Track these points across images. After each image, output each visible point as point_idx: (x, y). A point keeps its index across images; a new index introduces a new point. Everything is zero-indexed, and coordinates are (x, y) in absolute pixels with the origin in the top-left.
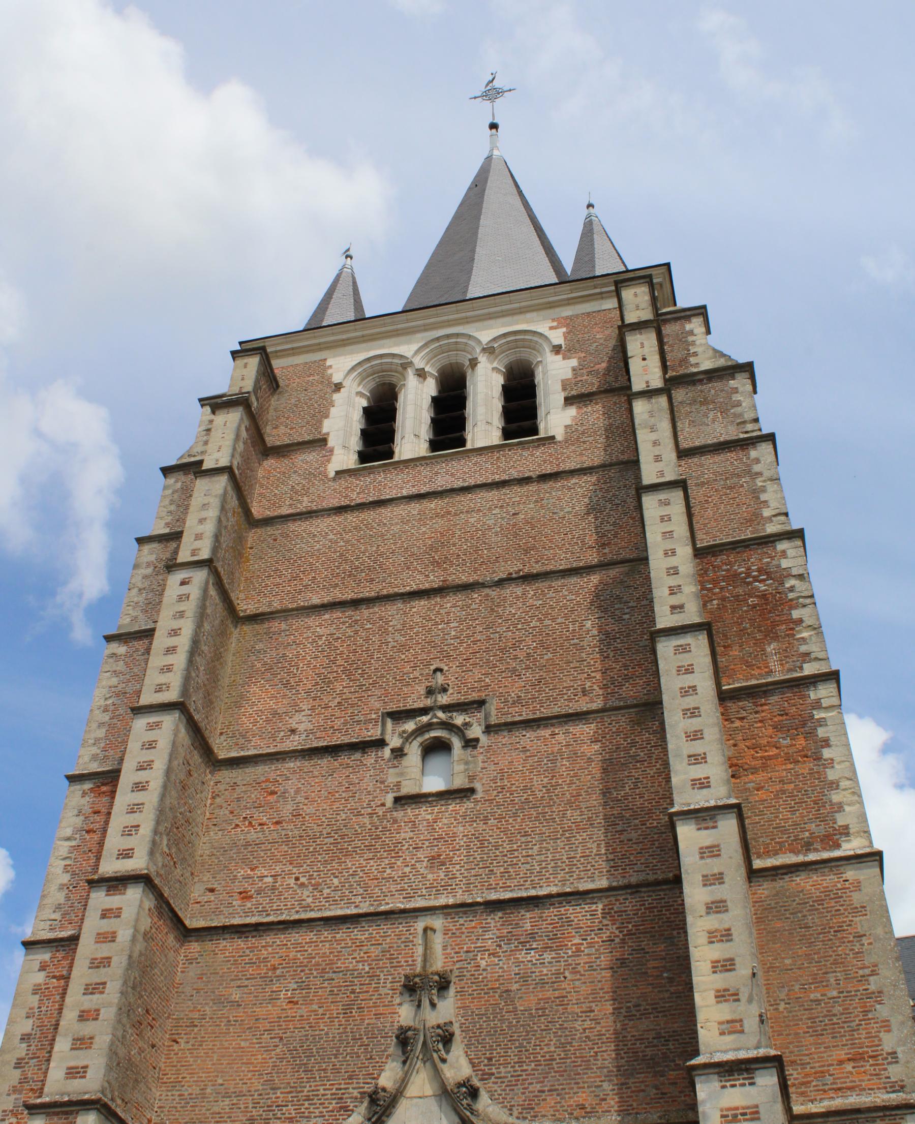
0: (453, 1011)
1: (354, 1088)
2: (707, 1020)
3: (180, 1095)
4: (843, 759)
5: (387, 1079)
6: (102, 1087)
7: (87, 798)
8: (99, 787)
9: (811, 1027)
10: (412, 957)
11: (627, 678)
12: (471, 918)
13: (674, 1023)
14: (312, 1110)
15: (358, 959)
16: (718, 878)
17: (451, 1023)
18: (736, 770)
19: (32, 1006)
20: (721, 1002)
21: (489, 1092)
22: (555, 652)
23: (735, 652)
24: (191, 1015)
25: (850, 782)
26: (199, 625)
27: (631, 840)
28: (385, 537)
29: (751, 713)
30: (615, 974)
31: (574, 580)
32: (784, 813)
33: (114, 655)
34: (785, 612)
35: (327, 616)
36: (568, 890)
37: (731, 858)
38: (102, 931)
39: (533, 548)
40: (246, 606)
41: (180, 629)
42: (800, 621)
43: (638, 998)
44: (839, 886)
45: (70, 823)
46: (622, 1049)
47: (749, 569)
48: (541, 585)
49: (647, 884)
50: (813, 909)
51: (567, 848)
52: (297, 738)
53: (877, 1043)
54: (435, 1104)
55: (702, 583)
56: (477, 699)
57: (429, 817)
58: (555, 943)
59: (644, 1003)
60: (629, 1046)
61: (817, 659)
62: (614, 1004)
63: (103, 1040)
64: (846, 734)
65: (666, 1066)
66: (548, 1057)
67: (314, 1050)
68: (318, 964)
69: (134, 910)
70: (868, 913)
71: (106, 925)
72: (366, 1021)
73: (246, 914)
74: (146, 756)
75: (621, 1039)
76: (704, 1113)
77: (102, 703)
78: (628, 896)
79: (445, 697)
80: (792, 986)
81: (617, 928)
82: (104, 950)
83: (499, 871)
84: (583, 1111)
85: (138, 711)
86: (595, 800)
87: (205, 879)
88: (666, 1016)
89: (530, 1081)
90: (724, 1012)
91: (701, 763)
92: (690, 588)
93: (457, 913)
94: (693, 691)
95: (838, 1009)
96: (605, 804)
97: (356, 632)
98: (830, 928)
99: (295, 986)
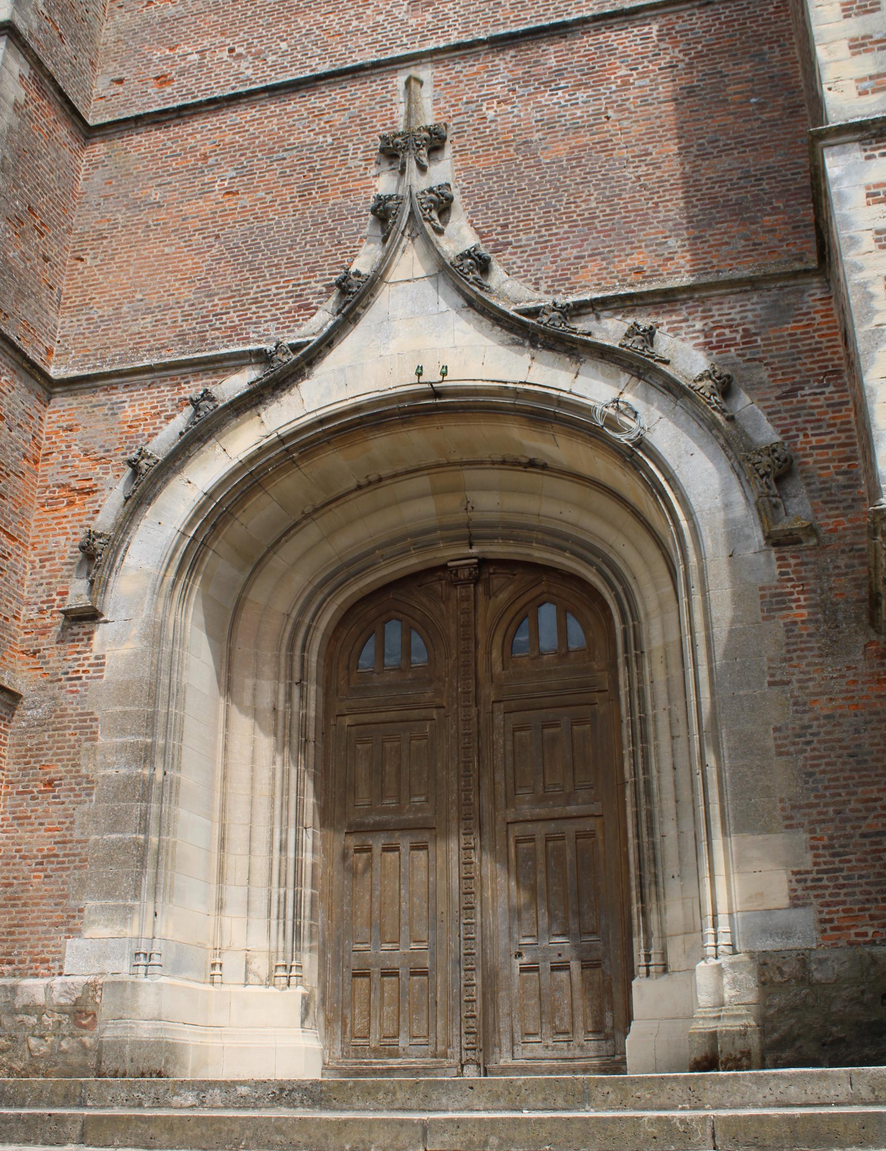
0: (450, 175)
1: (316, 282)
2: (838, 79)
3: (87, 320)
10: (391, 118)
12: (471, 63)
13: (768, 158)
14: (261, 314)
15: (317, 130)
17: (448, 185)
20: (859, 53)
21: (504, 265)
24: (98, 227)
30: (681, 107)
43: (714, 132)
46: (694, 196)
54: (430, 286)
59: (724, 137)
60: (704, 191)
62: (680, 143)
65: (759, 211)
66: (587, 215)
67: (262, 244)
68: (263, 144)
72: (331, 202)
75: (691, 183)
76: (840, 194)
78: (696, 11)
81: (680, 51)
87: (110, 70)
88: (756, 150)
89: (562, 246)
93: (452, 59)
99: (234, 174)
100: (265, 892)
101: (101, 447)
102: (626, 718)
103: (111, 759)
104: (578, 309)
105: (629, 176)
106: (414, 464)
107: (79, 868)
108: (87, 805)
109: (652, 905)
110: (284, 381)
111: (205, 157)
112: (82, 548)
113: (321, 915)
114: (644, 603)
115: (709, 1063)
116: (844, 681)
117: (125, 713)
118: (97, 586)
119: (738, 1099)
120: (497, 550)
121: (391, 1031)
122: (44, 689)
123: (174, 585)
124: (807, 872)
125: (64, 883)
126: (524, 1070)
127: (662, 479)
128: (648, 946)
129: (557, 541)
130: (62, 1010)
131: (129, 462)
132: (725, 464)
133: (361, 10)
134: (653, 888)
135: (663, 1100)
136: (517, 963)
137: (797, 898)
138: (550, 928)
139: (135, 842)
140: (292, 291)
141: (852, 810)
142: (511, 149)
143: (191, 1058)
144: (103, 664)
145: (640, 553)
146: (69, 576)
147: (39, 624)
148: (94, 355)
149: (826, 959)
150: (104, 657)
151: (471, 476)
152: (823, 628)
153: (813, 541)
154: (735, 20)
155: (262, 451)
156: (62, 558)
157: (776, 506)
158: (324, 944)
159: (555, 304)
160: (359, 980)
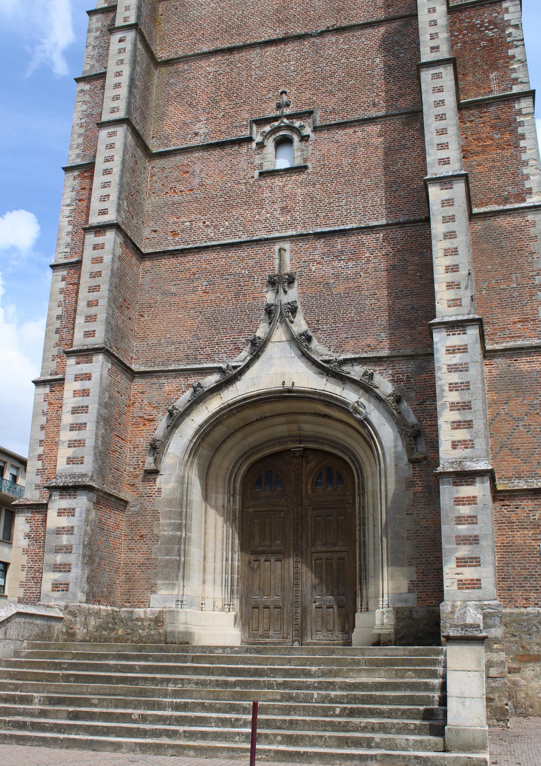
2: (441, 299)
3: (147, 344)
4: (532, 147)
5: (261, 332)
6: (104, 341)
7: (77, 181)
8: (83, 173)
9: (500, 304)
11: (401, 96)
16: (452, 218)
17: (296, 301)
18: (466, 153)
19: (60, 300)
20: (450, 289)
22: (356, 79)
23: (470, 78)
24: (149, 302)
25: (536, 161)
26: (133, 69)
27: (400, 196)
28: (247, 4)
29: (477, 118)
31: (369, 31)
32: (493, 180)
33: (82, 91)
34: (504, 51)
35: (213, 60)
36: (363, 226)
37: (460, 206)
38: (95, 257)
39: (343, 9)
40: (162, 55)
41: (122, 71)
42: (513, 57)
44: (523, 224)
45: (68, 196)
47: (483, 21)
48: (348, 35)
49: (410, 222)
50: (506, 237)
51: (362, 202)
52: (199, 138)
53: (536, 313)
55: (451, 32)
56: (308, 110)
57: (280, 184)
58: (355, 256)
60: (396, 313)
61: (522, 83)
63: (102, 316)
64: (535, 131)
68: (219, 271)
69: (112, 244)
70: (538, 240)
71: (97, 253)
72: (248, 302)
73: (176, 244)
74: (109, 153)
76: (437, 349)
77: (79, 121)
78: (398, 229)
79: (288, 110)
80: (491, 281)
81: (391, 248)
82: (97, 268)
83: (322, 215)
84: (370, 348)
85: (102, 125)
86: (380, 172)
88: (417, 297)
90: (452, 294)
91: (445, 149)
92: (444, 35)
93: (298, 240)
94: (442, 103)
95: (516, 294)
96: (386, 174)
97: (232, 69)
98: (515, 248)
99: (207, 283)
100: (220, 576)
101: (156, 402)
102: (358, 516)
103: (165, 528)
104: (345, 361)
105: (368, 304)
106: (279, 412)
107: (155, 569)
108: (157, 546)
109: (364, 587)
110: (230, 381)
111: (194, 274)
112: (151, 445)
113: (240, 585)
114: (366, 472)
115: (377, 643)
116: (432, 515)
117: (170, 511)
118: (157, 461)
119: (374, 654)
120: (311, 446)
121: (267, 628)
122: (137, 500)
123: (188, 460)
124: (415, 581)
125: (149, 574)
126: (316, 644)
127: (373, 433)
128: (362, 601)
129: (334, 445)
130: (151, 620)
131: (169, 411)
132: (396, 430)
133: (260, 210)
134: (364, 581)
135: (354, 654)
136: (314, 605)
137: (410, 589)
138: (326, 593)
139: (176, 560)
140: (232, 341)
141: (431, 560)
142: (321, 286)
143: (196, 638)
144: (161, 491)
145: (366, 453)
146: (146, 455)
147: (134, 473)
148: (151, 361)
149: (418, 611)
150: (161, 488)
151: (301, 418)
152: (426, 495)
153: (426, 462)
154: (413, 236)
155: (221, 409)
156: (142, 447)
157: (413, 448)
158: (242, 596)
159: (336, 360)
160: (255, 609)
